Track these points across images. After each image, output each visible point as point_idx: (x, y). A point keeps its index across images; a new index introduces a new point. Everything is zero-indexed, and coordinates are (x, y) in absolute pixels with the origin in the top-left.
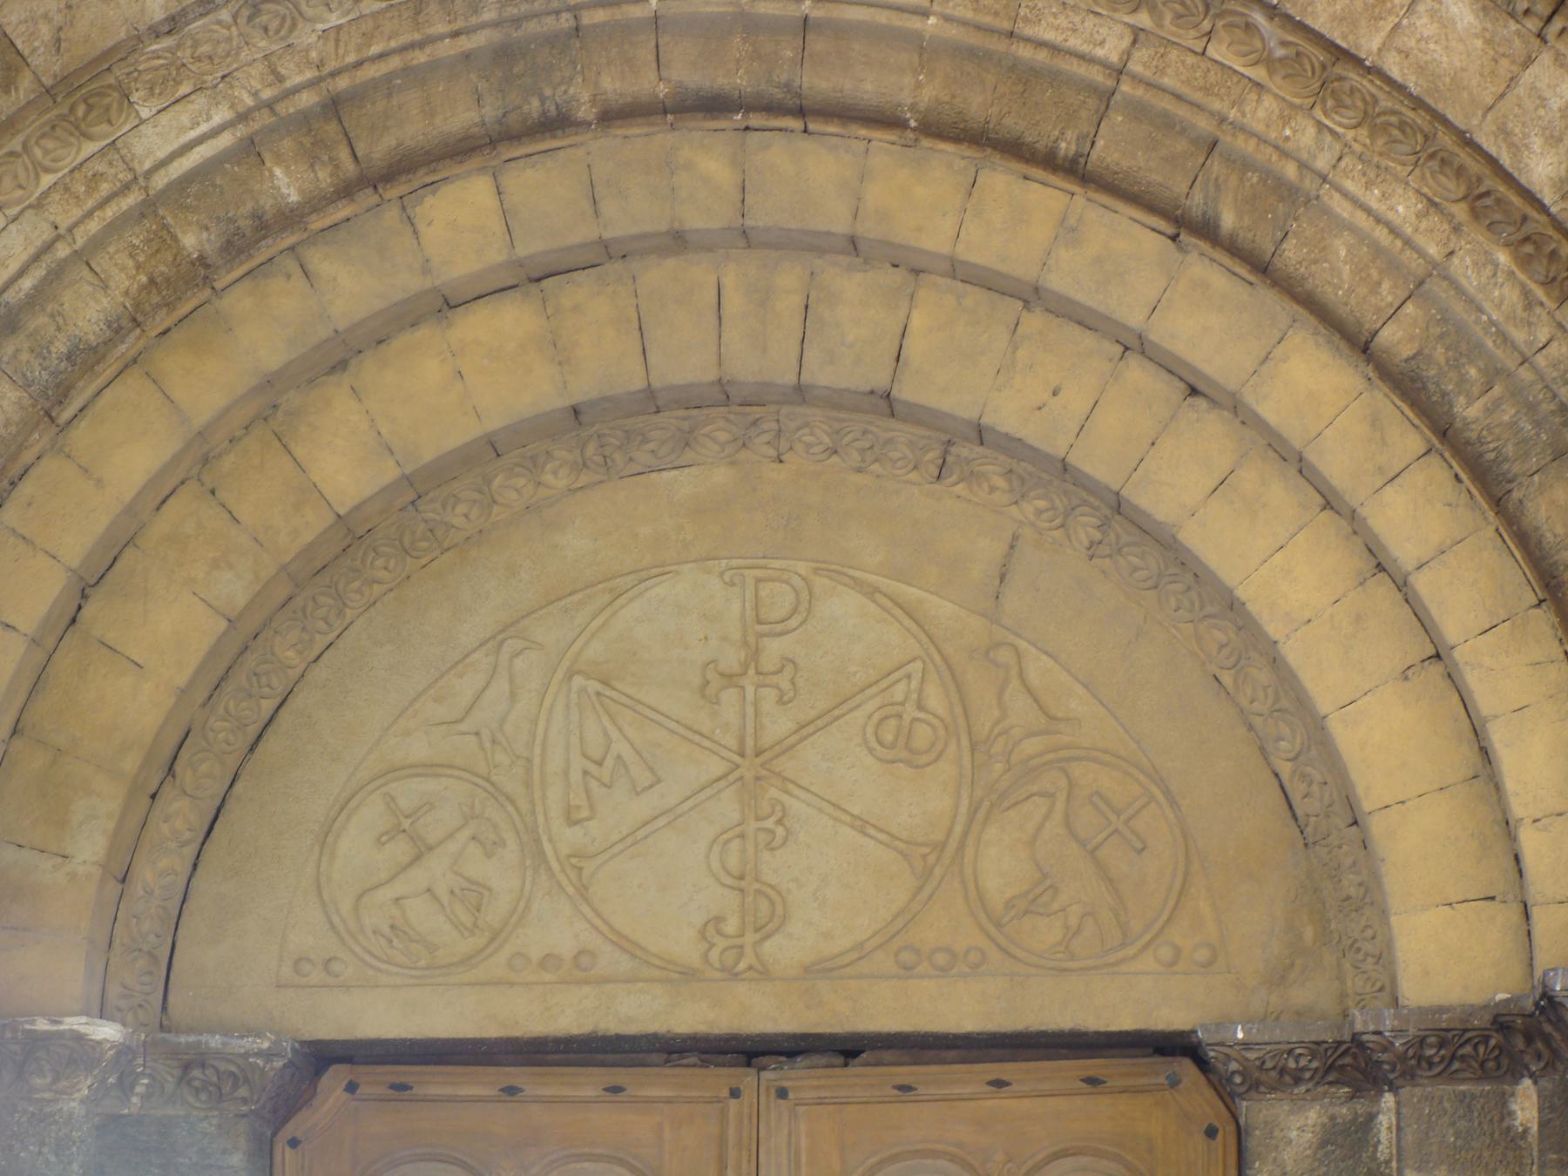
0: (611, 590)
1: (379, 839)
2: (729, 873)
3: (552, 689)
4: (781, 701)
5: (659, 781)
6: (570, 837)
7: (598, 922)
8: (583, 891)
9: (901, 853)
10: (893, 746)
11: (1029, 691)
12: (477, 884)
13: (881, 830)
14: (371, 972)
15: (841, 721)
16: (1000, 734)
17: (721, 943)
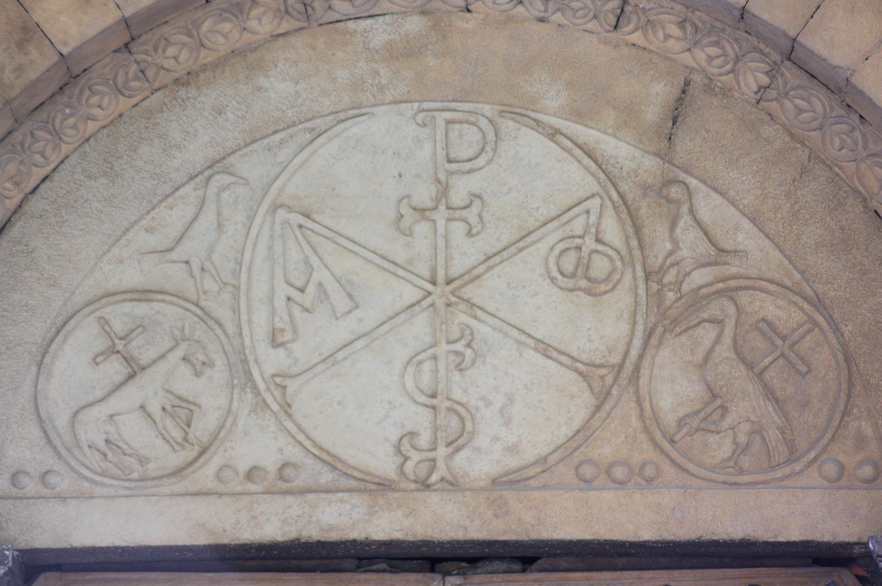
0: (313, 129)
1: (94, 359)
2: (422, 392)
3: (258, 221)
4: (470, 234)
5: (357, 307)
6: (271, 360)
7: (301, 437)
8: (286, 407)
9: (581, 373)
10: (573, 276)
11: (699, 224)
12: (187, 401)
13: (563, 353)
14: (86, 484)
15: (524, 253)
16: (673, 265)
17: (415, 456)
